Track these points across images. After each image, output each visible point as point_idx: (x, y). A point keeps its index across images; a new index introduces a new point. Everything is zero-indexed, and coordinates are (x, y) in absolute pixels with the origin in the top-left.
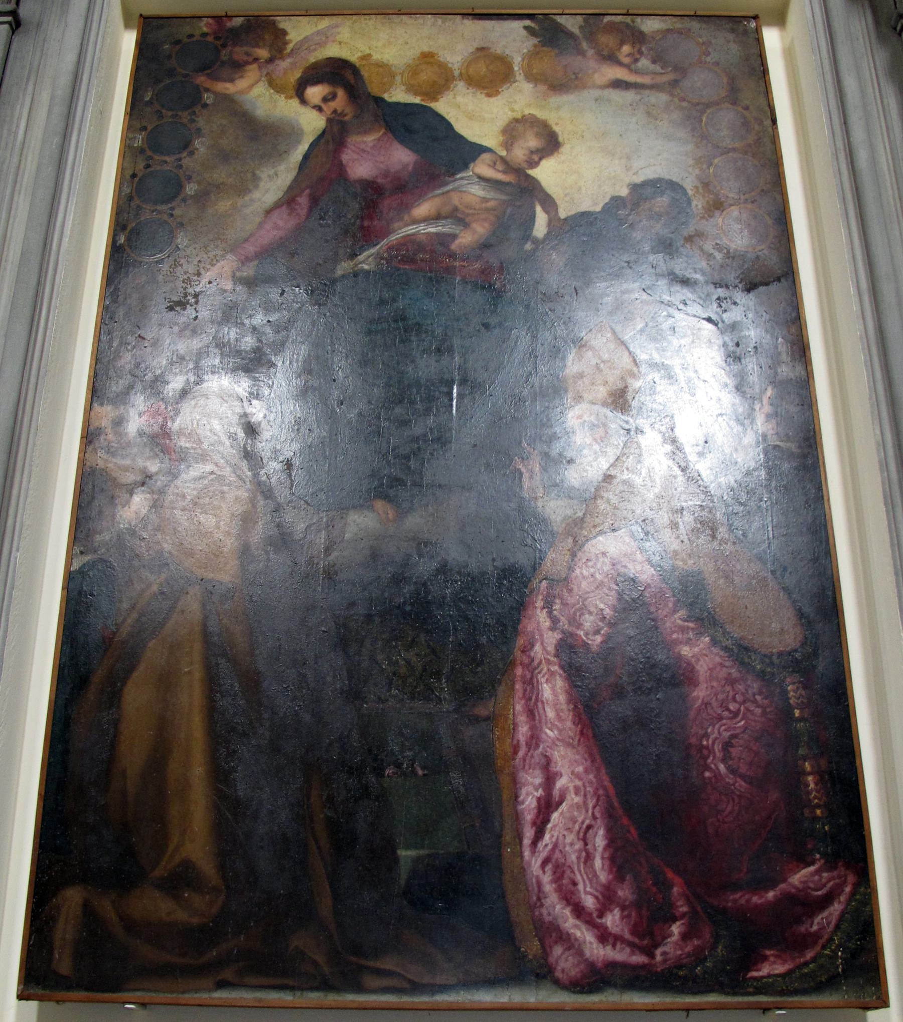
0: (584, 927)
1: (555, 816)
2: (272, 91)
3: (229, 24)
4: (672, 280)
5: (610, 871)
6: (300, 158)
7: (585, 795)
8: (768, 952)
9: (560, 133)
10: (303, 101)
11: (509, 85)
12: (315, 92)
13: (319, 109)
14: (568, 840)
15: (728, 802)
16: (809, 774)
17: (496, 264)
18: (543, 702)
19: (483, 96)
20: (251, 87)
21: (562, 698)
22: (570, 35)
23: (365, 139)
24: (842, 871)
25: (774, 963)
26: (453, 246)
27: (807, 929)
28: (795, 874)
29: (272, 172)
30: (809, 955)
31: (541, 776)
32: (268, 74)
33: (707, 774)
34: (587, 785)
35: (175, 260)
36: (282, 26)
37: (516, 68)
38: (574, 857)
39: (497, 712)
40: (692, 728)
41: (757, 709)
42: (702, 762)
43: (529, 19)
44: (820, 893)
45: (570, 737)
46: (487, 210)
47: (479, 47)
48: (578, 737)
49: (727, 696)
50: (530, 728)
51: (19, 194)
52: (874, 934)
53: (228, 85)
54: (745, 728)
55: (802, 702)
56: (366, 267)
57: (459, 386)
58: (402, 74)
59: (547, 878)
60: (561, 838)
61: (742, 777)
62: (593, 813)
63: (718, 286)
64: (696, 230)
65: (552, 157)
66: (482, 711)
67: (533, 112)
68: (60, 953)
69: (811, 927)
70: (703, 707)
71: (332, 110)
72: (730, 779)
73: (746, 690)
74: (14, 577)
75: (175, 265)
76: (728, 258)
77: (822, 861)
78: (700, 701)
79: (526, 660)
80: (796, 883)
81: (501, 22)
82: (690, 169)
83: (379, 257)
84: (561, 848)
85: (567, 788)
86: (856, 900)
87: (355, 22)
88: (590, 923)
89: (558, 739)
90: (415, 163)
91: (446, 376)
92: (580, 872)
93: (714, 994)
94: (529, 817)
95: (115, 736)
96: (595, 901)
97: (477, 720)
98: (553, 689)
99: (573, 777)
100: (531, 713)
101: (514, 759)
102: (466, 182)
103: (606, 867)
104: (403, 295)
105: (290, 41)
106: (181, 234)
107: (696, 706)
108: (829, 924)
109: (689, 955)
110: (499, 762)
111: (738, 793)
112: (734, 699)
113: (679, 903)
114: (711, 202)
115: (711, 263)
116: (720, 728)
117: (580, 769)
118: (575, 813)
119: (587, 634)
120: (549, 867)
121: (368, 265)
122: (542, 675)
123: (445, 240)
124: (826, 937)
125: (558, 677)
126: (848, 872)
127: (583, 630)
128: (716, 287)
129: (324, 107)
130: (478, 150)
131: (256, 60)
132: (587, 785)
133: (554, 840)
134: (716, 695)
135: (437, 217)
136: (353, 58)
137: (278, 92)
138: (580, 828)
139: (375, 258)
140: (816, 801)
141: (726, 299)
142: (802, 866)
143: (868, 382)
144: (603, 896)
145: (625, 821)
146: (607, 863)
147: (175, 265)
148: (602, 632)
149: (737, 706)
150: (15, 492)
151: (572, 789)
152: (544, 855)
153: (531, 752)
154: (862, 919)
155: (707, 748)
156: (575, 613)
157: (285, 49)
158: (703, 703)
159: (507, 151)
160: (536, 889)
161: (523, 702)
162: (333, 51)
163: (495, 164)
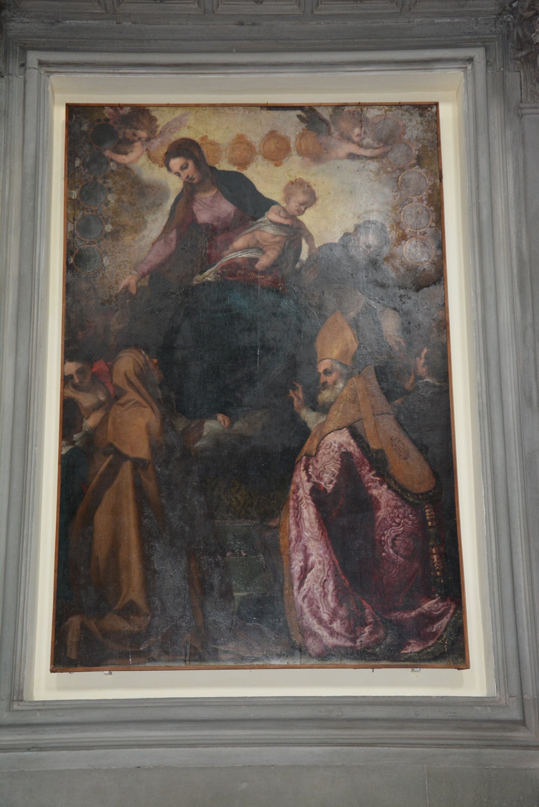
0: (323, 629)
1: (309, 575)
2: (150, 162)
3: (122, 112)
4: (376, 285)
5: (336, 601)
7: (324, 565)
8: (411, 641)
9: (316, 191)
10: (169, 169)
11: (288, 158)
12: (176, 163)
14: (315, 587)
15: (394, 568)
16: (435, 554)
17: (280, 277)
18: (303, 519)
19: (273, 166)
20: (138, 158)
22: (323, 121)
23: (206, 196)
24: (449, 602)
25: (414, 646)
26: (257, 266)
27: (430, 630)
28: (426, 603)
29: (154, 217)
30: (431, 643)
31: (302, 555)
32: (147, 149)
33: (384, 554)
35: (103, 274)
36: (153, 114)
37: (292, 146)
38: (318, 595)
41: (409, 522)
43: (300, 110)
44: (437, 613)
49: (395, 515)
51: (11, 234)
52: (463, 633)
54: (403, 531)
56: (209, 279)
57: (261, 349)
58: (226, 150)
59: (305, 605)
60: (312, 586)
61: (401, 556)
62: (327, 573)
63: (401, 288)
64: (391, 253)
66: (273, 524)
67: (302, 177)
68: (70, 649)
69: (432, 629)
70: (383, 520)
71: (186, 175)
73: (405, 512)
75: (103, 277)
76: (408, 271)
77: (439, 597)
78: (381, 517)
80: (426, 608)
81: (283, 111)
83: (216, 273)
85: (315, 561)
86: (455, 617)
87: (197, 112)
88: (326, 627)
89: (311, 537)
91: (254, 345)
92: (321, 602)
96: (328, 616)
97: (270, 528)
98: (308, 512)
100: (297, 524)
101: (289, 547)
102: (263, 224)
104: (230, 296)
108: (441, 628)
109: (373, 642)
110: (282, 549)
111: (399, 564)
113: (369, 617)
114: (400, 235)
115: (398, 274)
116: (390, 531)
117: (321, 552)
119: (325, 484)
120: (306, 600)
121: (210, 277)
124: (439, 634)
125: (311, 506)
126: (452, 603)
128: (399, 289)
129: (182, 174)
130: (269, 203)
131: (140, 139)
132: (325, 560)
133: (309, 586)
136: (197, 139)
137: (154, 162)
138: (321, 581)
140: (437, 568)
141: (404, 296)
142: (429, 600)
143: (476, 348)
144: (332, 613)
146: (334, 597)
147: (103, 277)
150: (31, 414)
151: (317, 561)
152: (304, 594)
153: (298, 543)
154: (458, 626)
155: (384, 541)
156: (319, 473)
157: (156, 131)
158: (382, 519)
160: (300, 611)
161: (293, 519)
162: (184, 133)
163: (280, 213)
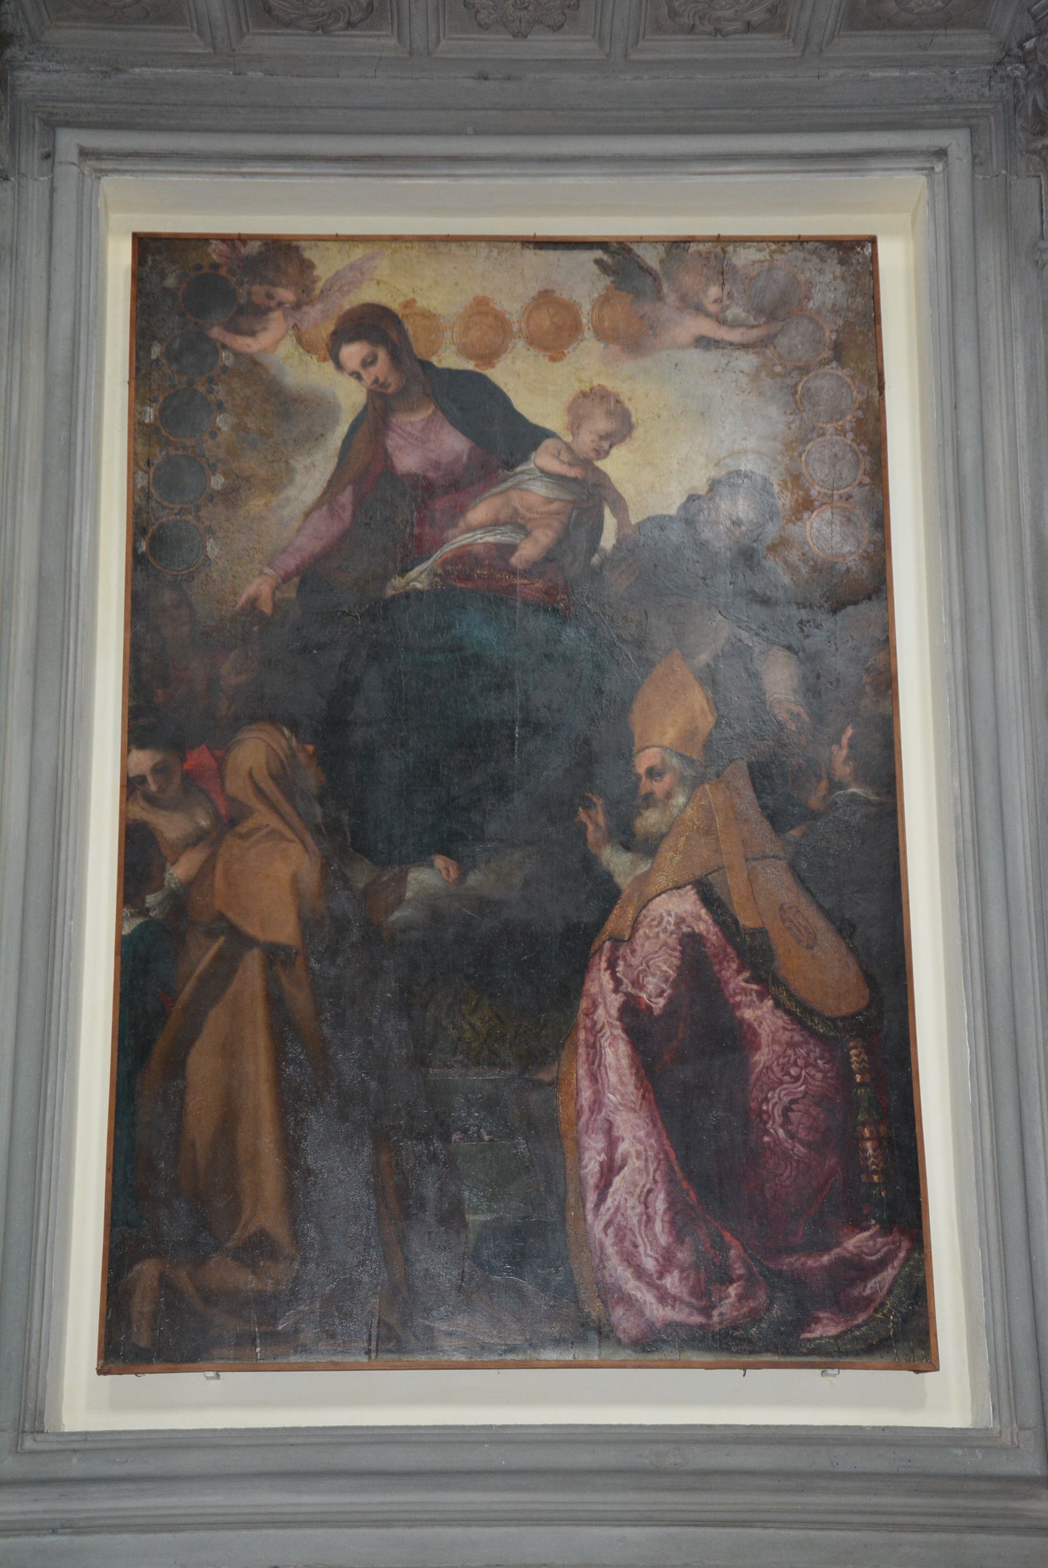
1: (617, 1180)
2: (301, 350)
3: (245, 251)
4: (751, 600)
5: (670, 1233)
6: (339, 443)
7: (646, 1160)
8: (821, 1315)
9: (633, 413)
10: (339, 366)
11: (576, 344)
12: (353, 353)
13: (358, 376)
14: (629, 1204)
18: (605, 1067)
19: (547, 360)
20: (277, 343)
21: (625, 1062)
25: (827, 1325)
26: (514, 560)
28: (850, 1239)
30: (861, 1318)
31: (603, 1140)
32: (295, 326)
34: (648, 1149)
36: (307, 254)
37: (584, 321)
38: (635, 1221)
39: (560, 1076)
40: (752, 1092)
42: (761, 1126)
44: (874, 1258)
45: (632, 1101)
46: (550, 514)
47: (542, 289)
48: (639, 1102)
49: (789, 1060)
50: (593, 1092)
53: (249, 340)
54: (806, 1093)
55: (864, 1067)
56: (419, 586)
57: (521, 727)
58: (452, 328)
59: (609, 1241)
60: (623, 1202)
62: (654, 1177)
65: (623, 444)
66: (545, 1076)
69: (864, 1290)
70: (765, 1071)
71: (373, 378)
72: (788, 1144)
73: (808, 1054)
74: (70, 943)
75: (207, 581)
77: (878, 1227)
78: (761, 1065)
79: (589, 1024)
80: (851, 1248)
82: (779, 458)
84: (622, 1211)
87: (395, 251)
88: (651, 1285)
89: (621, 1104)
90: (471, 449)
92: (641, 1234)
93: (769, 1354)
94: (592, 1181)
95: (182, 1108)
97: (539, 1085)
98: (616, 1053)
99: (635, 1141)
100: (594, 1078)
102: (527, 477)
103: (666, 1230)
105: (318, 278)
106: (211, 540)
107: (757, 1070)
109: (745, 1316)
110: (563, 1127)
111: (795, 1158)
112: (795, 1064)
113: (736, 1266)
115: (795, 578)
117: (642, 1134)
118: (637, 1177)
119: (650, 997)
120: (611, 1231)
122: (604, 1038)
123: (508, 549)
124: (878, 1301)
125: (620, 1041)
127: (646, 992)
128: (798, 608)
130: (542, 435)
131: (280, 304)
133: (616, 1203)
134: (778, 1059)
135: (494, 524)
136: (395, 306)
137: (308, 352)
138: (641, 1192)
139: (429, 574)
140: (874, 1167)
141: (809, 621)
142: (857, 1231)
144: (664, 1258)
145: (685, 1185)
146: (667, 1225)
147: (207, 581)
148: (665, 995)
149: (798, 1070)
151: (633, 1153)
152: (607, 1218)
154: (915, 1284)
155: (767, 1112)
156: (638, 976)
157: (313, 289)
159: (573, 436)
161: (586, 1066)
162: (369, 294)
163: (559, 454)
